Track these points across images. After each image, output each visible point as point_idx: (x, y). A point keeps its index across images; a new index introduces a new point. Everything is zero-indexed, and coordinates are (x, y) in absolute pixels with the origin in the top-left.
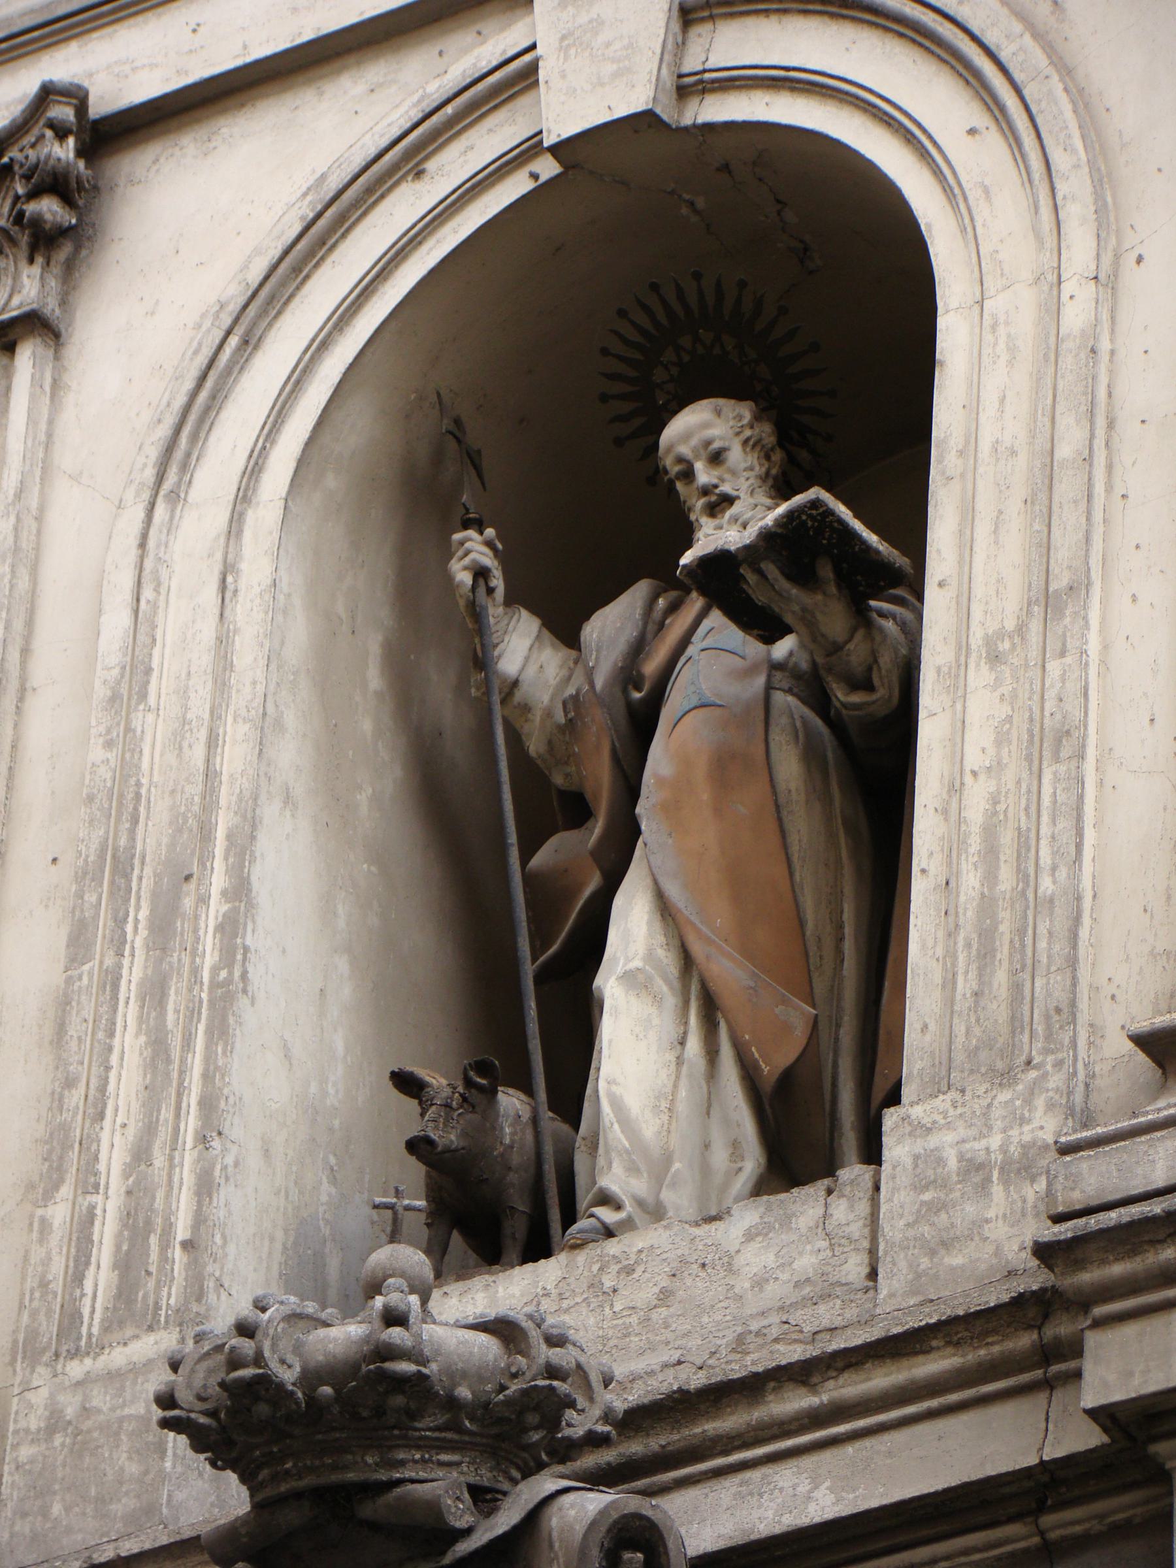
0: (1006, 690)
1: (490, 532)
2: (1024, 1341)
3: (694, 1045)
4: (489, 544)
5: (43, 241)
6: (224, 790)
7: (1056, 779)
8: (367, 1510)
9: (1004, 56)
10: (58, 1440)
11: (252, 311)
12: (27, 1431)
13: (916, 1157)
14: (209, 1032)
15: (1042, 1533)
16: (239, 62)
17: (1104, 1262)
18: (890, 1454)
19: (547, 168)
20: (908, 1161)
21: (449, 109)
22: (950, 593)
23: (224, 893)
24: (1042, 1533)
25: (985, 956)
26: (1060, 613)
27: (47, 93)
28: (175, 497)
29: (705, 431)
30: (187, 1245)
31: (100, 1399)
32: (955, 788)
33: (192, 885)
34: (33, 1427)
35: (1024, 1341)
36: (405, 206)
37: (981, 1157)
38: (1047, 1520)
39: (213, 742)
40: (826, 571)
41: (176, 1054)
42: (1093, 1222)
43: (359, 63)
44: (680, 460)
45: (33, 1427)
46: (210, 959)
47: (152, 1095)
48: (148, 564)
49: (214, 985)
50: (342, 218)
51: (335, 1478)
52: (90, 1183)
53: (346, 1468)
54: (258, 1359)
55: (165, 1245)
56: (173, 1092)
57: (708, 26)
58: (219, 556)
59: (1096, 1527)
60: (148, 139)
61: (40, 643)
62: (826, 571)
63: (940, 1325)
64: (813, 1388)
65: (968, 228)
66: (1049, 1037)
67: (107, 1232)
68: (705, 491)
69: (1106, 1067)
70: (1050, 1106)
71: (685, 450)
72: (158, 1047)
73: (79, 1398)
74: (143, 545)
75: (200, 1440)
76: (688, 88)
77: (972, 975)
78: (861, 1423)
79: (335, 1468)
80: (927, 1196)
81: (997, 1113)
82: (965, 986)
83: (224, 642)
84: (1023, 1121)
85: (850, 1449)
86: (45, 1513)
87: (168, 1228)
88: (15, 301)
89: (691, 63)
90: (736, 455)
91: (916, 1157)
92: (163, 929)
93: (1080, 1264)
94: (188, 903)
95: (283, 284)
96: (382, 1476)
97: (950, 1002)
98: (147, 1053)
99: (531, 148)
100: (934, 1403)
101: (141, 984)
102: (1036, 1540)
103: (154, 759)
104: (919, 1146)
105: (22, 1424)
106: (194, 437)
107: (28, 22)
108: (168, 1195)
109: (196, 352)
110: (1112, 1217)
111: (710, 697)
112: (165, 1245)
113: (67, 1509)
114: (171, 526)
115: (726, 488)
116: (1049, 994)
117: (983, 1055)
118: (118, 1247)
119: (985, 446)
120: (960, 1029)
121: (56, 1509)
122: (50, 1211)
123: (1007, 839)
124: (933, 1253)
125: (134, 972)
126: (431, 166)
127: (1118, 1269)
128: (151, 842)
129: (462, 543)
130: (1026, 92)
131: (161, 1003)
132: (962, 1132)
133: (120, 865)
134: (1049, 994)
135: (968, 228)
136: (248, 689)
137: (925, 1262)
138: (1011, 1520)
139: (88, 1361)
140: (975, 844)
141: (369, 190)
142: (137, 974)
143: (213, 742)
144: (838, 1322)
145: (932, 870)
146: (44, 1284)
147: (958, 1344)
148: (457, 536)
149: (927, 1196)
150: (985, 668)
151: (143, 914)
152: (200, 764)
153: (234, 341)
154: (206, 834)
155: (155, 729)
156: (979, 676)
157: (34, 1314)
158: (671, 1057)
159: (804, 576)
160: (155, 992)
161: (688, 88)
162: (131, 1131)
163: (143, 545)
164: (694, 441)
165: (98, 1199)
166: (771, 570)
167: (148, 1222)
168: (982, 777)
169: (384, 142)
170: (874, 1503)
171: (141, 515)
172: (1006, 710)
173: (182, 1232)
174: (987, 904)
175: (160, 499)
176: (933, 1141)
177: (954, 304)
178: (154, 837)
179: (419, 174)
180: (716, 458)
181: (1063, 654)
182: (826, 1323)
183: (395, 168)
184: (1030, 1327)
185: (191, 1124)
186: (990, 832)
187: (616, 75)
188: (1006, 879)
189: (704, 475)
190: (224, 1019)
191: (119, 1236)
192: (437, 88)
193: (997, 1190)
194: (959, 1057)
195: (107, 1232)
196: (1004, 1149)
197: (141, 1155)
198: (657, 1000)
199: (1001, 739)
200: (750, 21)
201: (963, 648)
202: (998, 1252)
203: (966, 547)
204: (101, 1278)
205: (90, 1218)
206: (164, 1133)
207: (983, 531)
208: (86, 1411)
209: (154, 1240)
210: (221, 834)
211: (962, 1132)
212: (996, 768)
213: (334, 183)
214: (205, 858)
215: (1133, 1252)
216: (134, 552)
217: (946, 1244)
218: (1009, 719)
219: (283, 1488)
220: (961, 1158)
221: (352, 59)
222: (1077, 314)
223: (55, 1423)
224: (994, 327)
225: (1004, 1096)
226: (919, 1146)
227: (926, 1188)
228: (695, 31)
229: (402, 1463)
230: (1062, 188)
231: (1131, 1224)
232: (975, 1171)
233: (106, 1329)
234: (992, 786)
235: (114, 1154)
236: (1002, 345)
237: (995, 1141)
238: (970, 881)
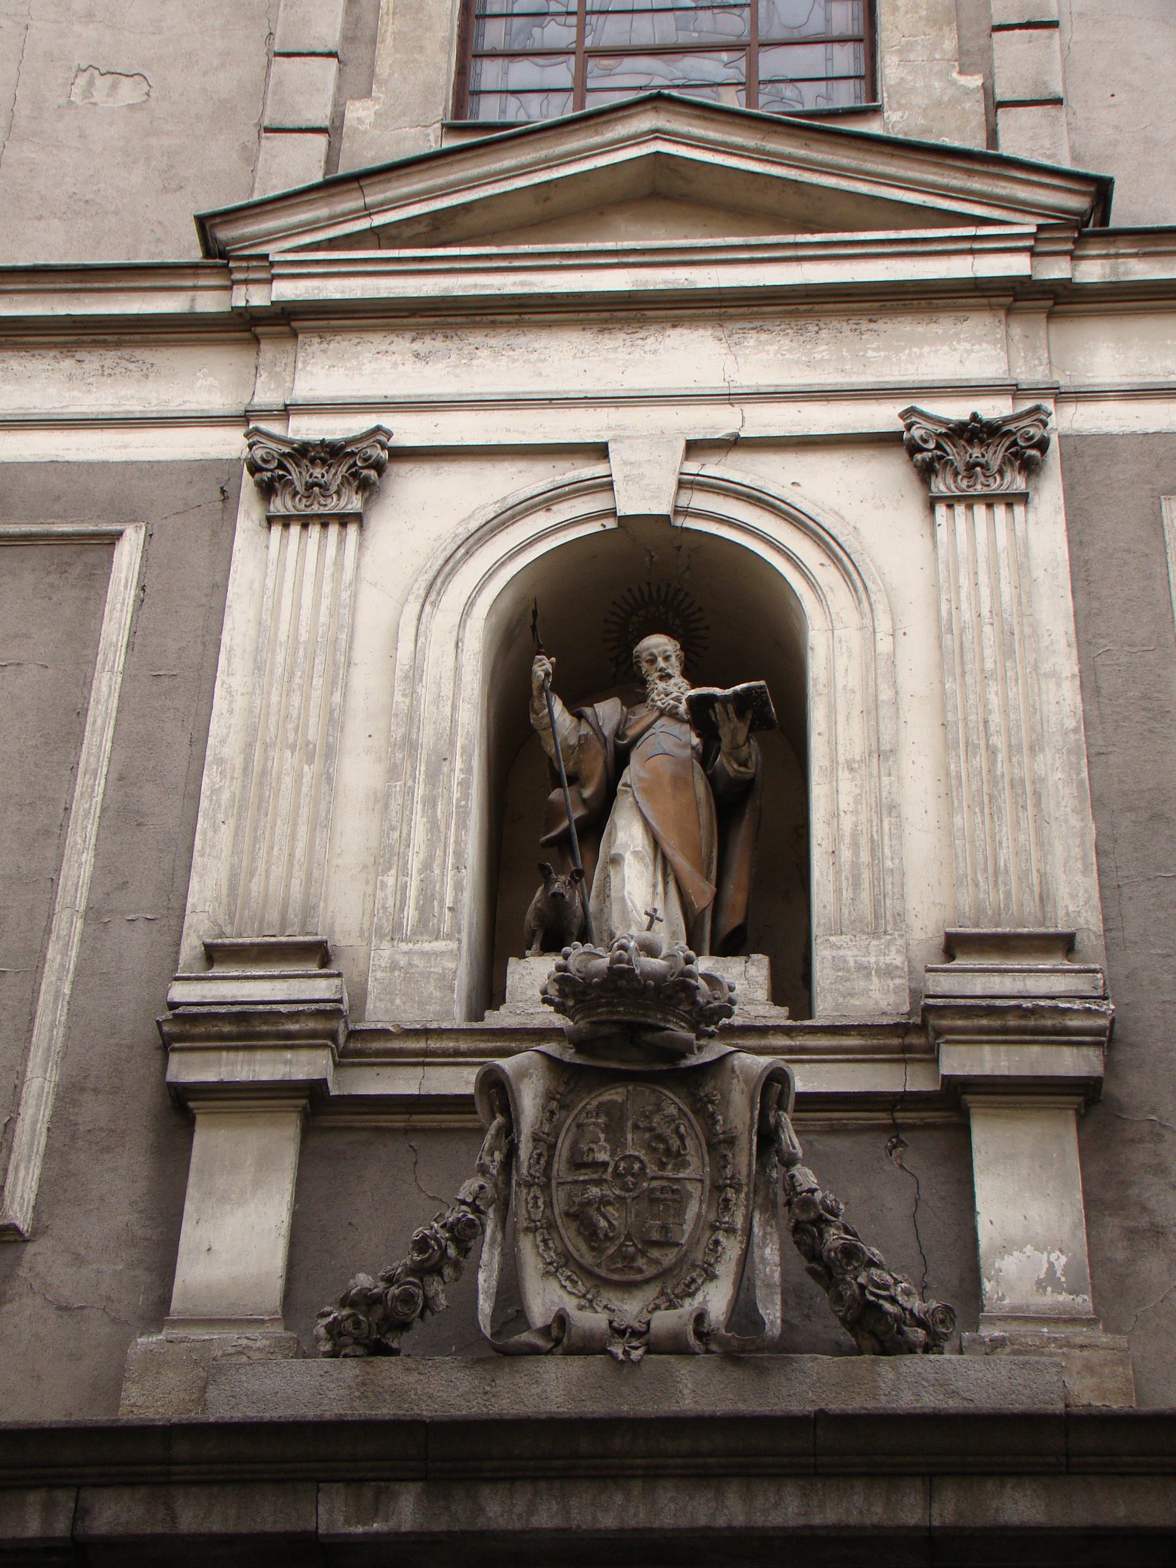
0: (858, 782)
1: (553, 659)
2: (896, 1041)
3: (660, 888)
4: (552, 663)
5: (364, 486)
6: (459, 729)
7: (890, 823)
8: (648, 1037)
9: (840, 540)
10: (397, 973)
11: (471, 541)
12: (380, 966)
13: (834, 957)
14: (457, 825)
15: (894, 1119)
16: (460, 444)
17: (953, 1018)
18: (828, 1072)
19: (611, 524)
20: (830, 958)
21: (567, 489)
22: (825, 738)
23: (461, 770)
24: (894, 1119)
25: (856, 884)
26: (886, 760)
27: (378, 429)
28: (434, 604)
29: (658, 644)
30: (450, 909)
31: (416, 960)
32: (835, 814)
33: (447, 763)
34: (383, 965)
35: (896, 1041)
36: (540, 521)
37: (866, 964)
38: (897, 1115)
39: (454, 708)
40: (749, 715)
41: (442, 829)
42: (953, 1002)
43: (513, 460)
44: (652, 654)
45: (383, 965)
46: (456, 795)
47: (431, 844)
48: (422, 628)
49: (458, 806)
50: (513, 516)
51: (643, 1019)
52: (404, 871)
53: (648, 1017)
54: (629, 962)
55: (441, 908)
56: (442, 844)
57: (689, 492)
58: (455, 633)
59: (919, 1122)
60: (407, 461)
61: (357, 645)
62: (749, 715)
63: (859, 1025)
64: (791, 1038)
65: (821, 599)
66: (895, 924)
67: (412, 893)
68: (661, 670)
69: (915, 943)
70: (898, 952)
71: (655, 651)
72: (433, 826)
73: (406, 958)
74: (419, 619)
75: (910, 991)
76: (677, 511)
77: (850, 891)
78: (814, 1057)
79: (644, 1015)
80: (840, 974)
81: (872, 949)
82: (847, 894)
83: (457, 669)
84: (885, 954)
85: (807, 1066)
86: (392, 1002)
87: (442, 901)
88: (349, 507)
89: (683, 502)
90: (673, 659)
91: (834, 957)
92: (433, 777)
93: (942, 1017)
94: (445, 769)
95: (486, 534)
96: (662, 1024)
97: (839, 899)
98: (428, 825)
99: (612, 513)
100: (851, 1057)
101: (422, 796)
102: (890, 1121)
103: (426, 709)
104: (834, 953)
105: (377, 963)
106: (443, 583)
107: (353, 401)
108: (442, 886)
109: (444, 550)
110: (962, 1002)
111: (667, 750)
112: (441, 908)
113: (404, 1003)
114: (432, 615)
115: (669, 671)
116: (894, 907)
117: (858, 924)
118: (418, 902)
119: (839, 686)
120: (845, 911)
121: (398, 1001)
122: (385, 879)
123: (864, 841)
124: (844, 997)
125: (420, 791)
126: (554, 508)
127: (960, 1023)
128: (425, 740)
129: (540, 660)
130: (852, 557)
131: (434, 806)
132: (856, 952)
133: (410, 745)
134: (894, 907)
135: (821, 599)
136: (469, 690)
137: (841, 1000)
138: (878, 1111)
139: (410, 945)
140: (847, 840)
141: (527, 509)
142: (421, 792)
143: (454, 708)
144: (767, 1014)
145: (824, 844)
146: (384, 908)
147: (863, 1036)
148: (538, 657)
149: (840, 974)
150: (846, 772)
151: (423, 768)
152: (449, 714)
153: (462, 551)
154: (452, 744)
155: (426, 694)
156: (844, 775)
157: (380, 919)
158: (651, 890)
159: (740, 715)
160: (431, 802)
161: (677, 511)
162: (421, 855)
163: (419, 619)
164: (660, 649)
165: (408, 879)
166: (730, 708)
167: (433, 895)
168: (849, 814)
169: (535, 493)
170: (824, 1090)
171: (419, 608)
172: (858, 791)
173: (449, 902)
174: (855, 865)
175: (427, 603)
176: (841, 952)
177: (816, 627)
178: (426, 737)
179: (548, 510)
180: (667, 658)
181: (890, 775)
182: (761, 1014)
183: (539, 504)
184: (898, 1037)
185: (451, 860)
186: (855, 836)
187: (652, 497)
188: (865, 857)
189: (661, 663)
190: (464, 821)
191: (417, 897)
192: (560, 479)
193: (875, 979)
194: (846, 922)
195: (412, 893)
196: (877, 963)
197: (427, 866)
198: (646, 866)
199: (857, 801)
200: (710, 495)
201: (834, 761)
202: (876, 1003)
203: (832, 722)
204: (411, 914)
205: (405, 887)
206: (438, 861)
207: (841, 719)
208: (410, 964)
209: (436, 903)
210: (459, 745)
211: (856, 952)
212: (855, 812)
213: (511, 502)
214: (453, 754)
215: (967, 1017)
216: (415, 622)
217: (852, 995)
218: (860, 794)
219: (615, 1017)
220: (856, 962)
221: (509, 457)
222: (884, 646)
223: (394, 966)
224: (840, 641)
225: (875, 942)
226: (834, 953)
227: (840, 970)
228: (682, 492)
229: (669, 1021)
230: (873, 598)
231: (965, 1006)
232: (864, 970)
233: (414, 933)
234: (854, 819)
235: (415, 864)
236: (844, 649)
237: (872, 959)
238: (846, 854)
